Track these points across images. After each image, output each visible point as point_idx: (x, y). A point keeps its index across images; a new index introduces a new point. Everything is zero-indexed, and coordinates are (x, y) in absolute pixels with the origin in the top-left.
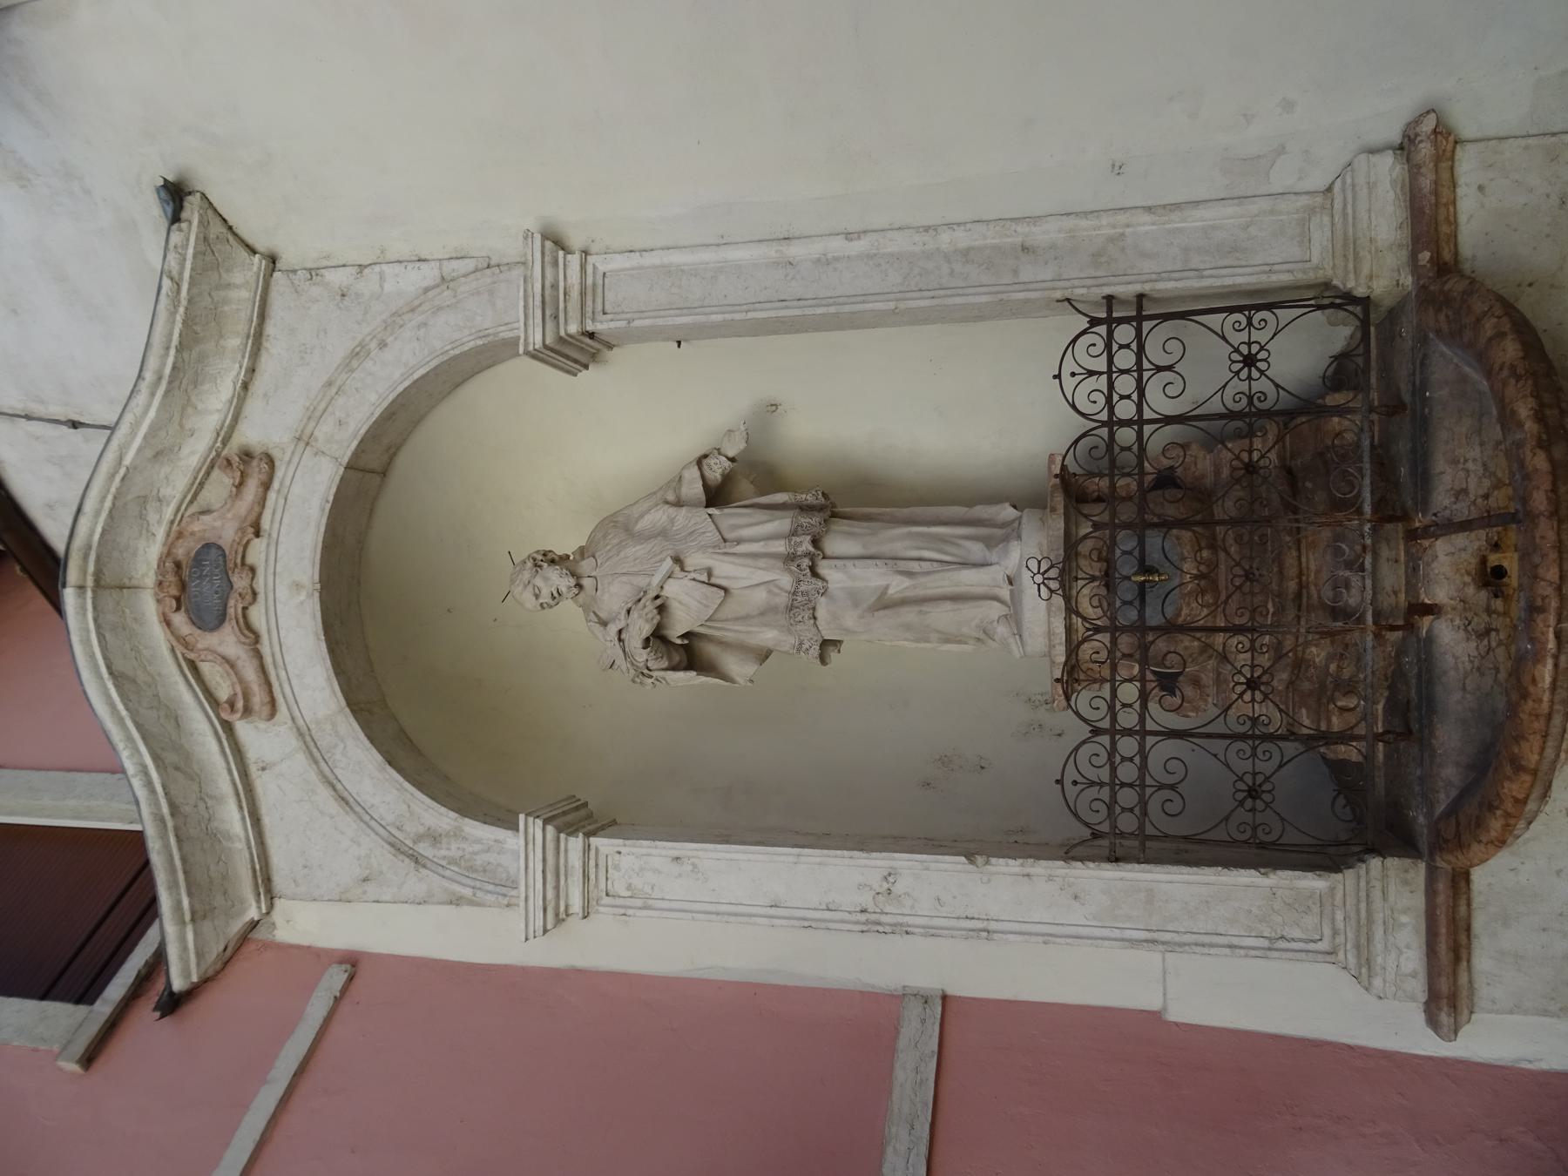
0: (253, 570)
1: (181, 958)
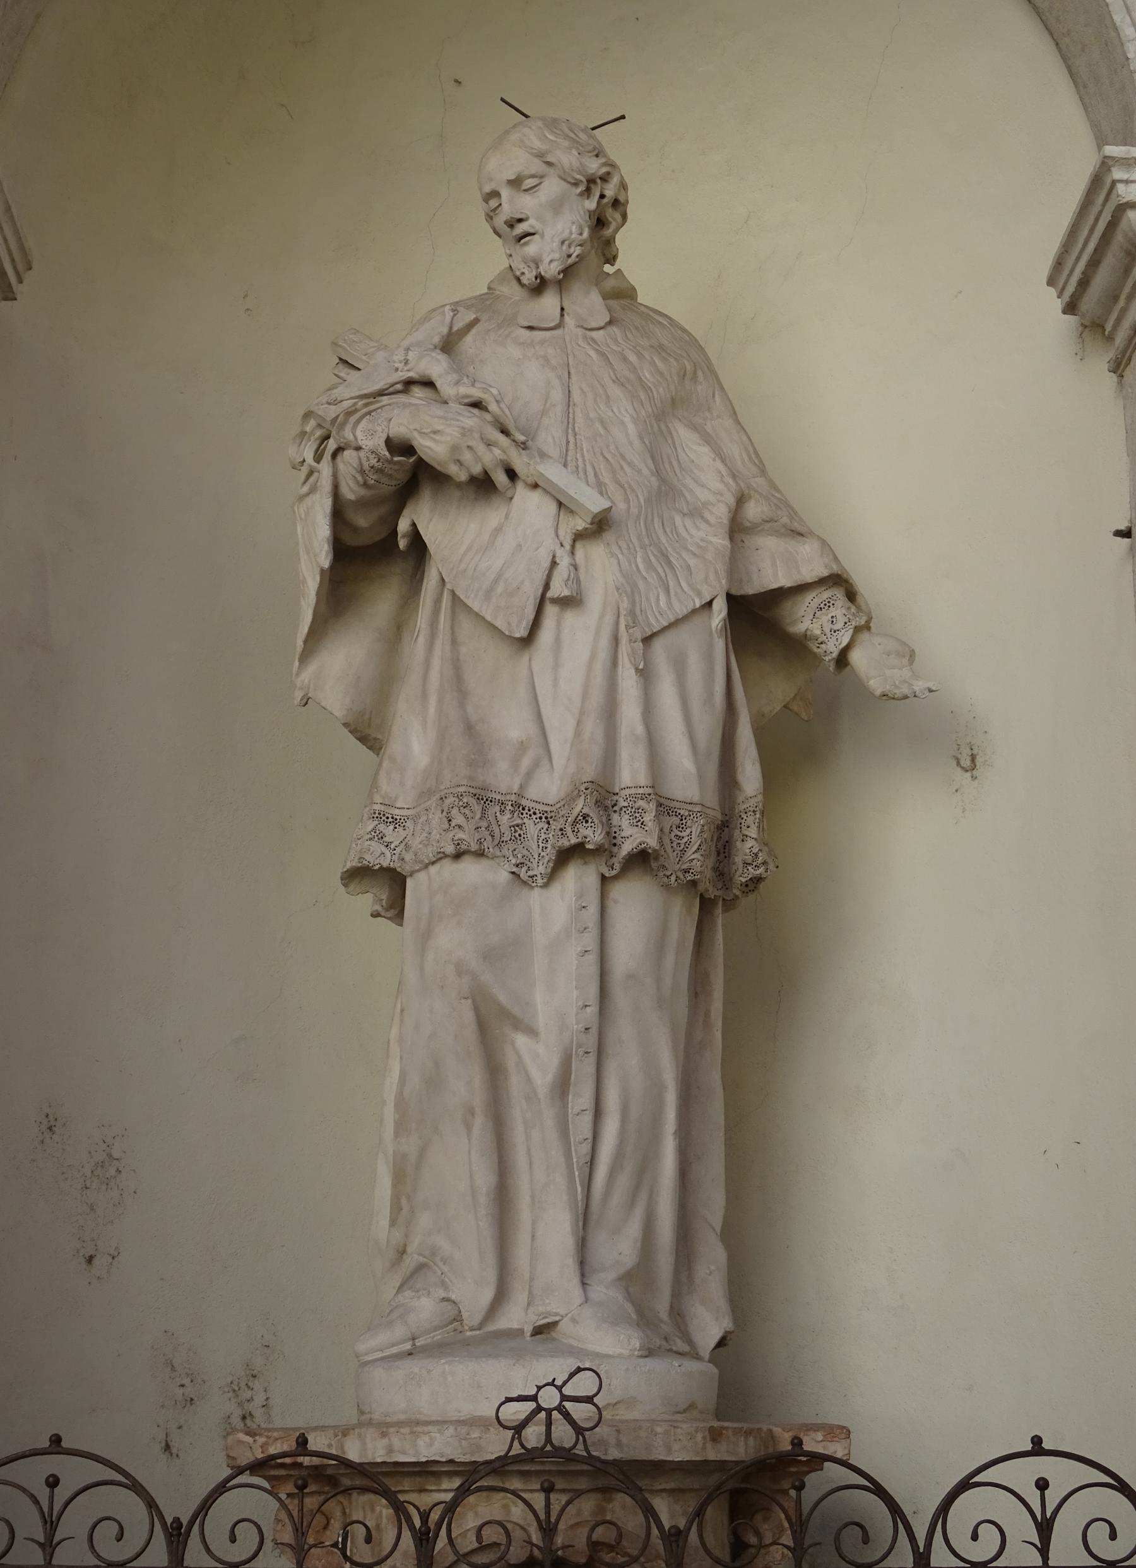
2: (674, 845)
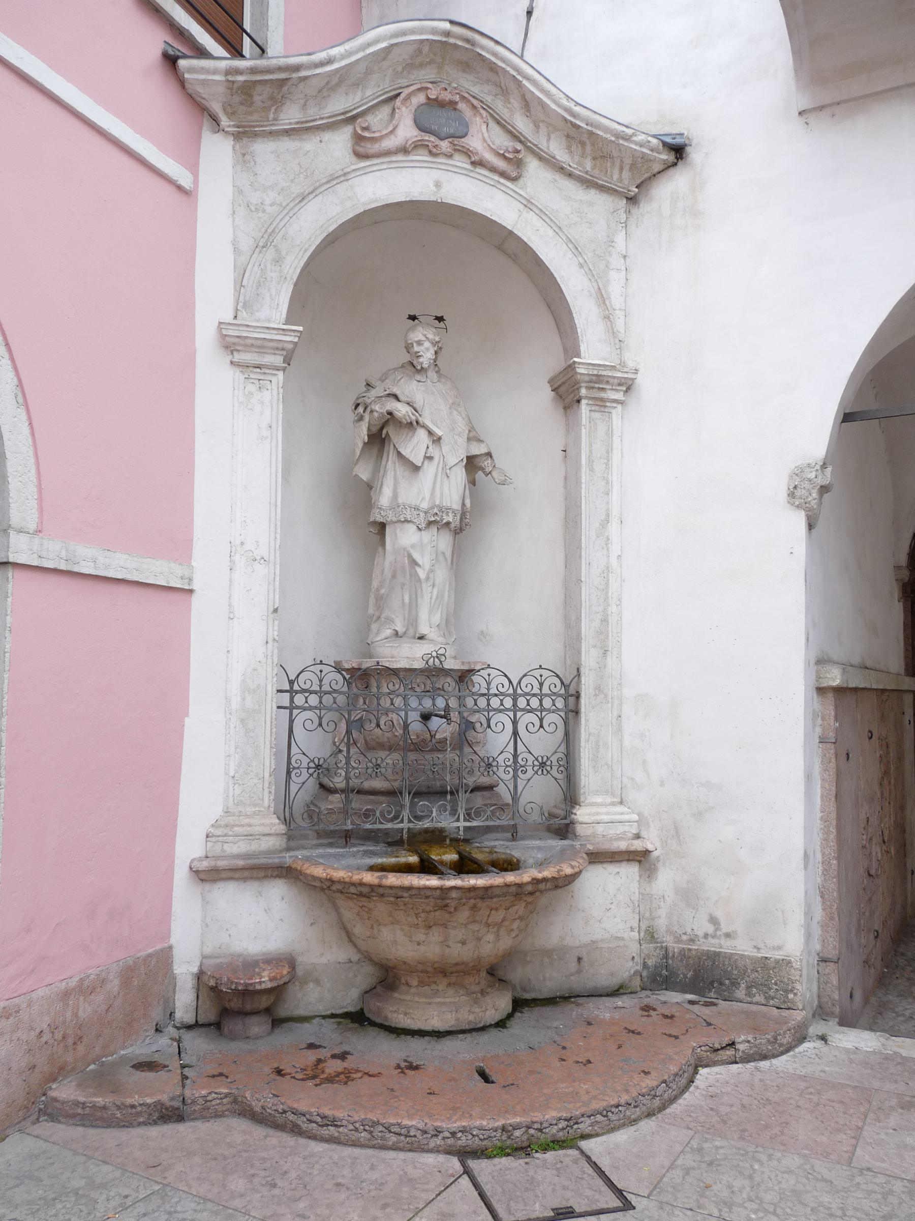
0: (450, 156)
1: (202, 68)
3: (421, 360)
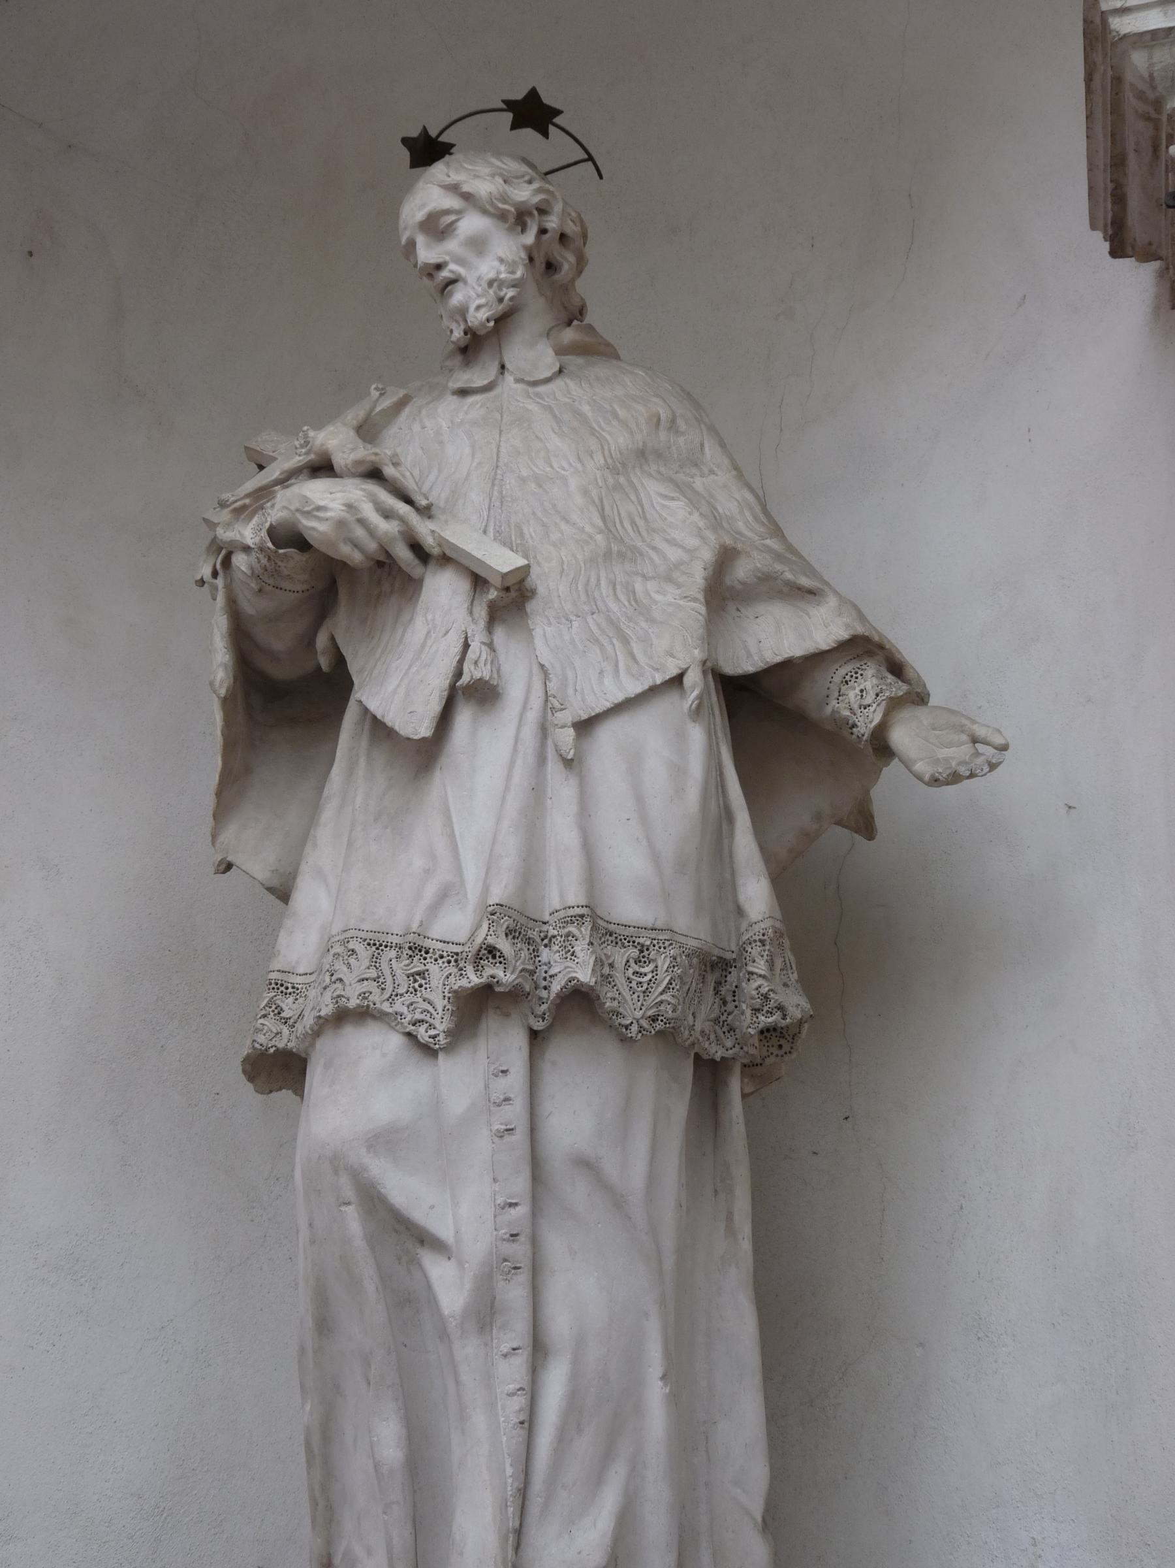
2: (634, 984)
3: (458, 296)
